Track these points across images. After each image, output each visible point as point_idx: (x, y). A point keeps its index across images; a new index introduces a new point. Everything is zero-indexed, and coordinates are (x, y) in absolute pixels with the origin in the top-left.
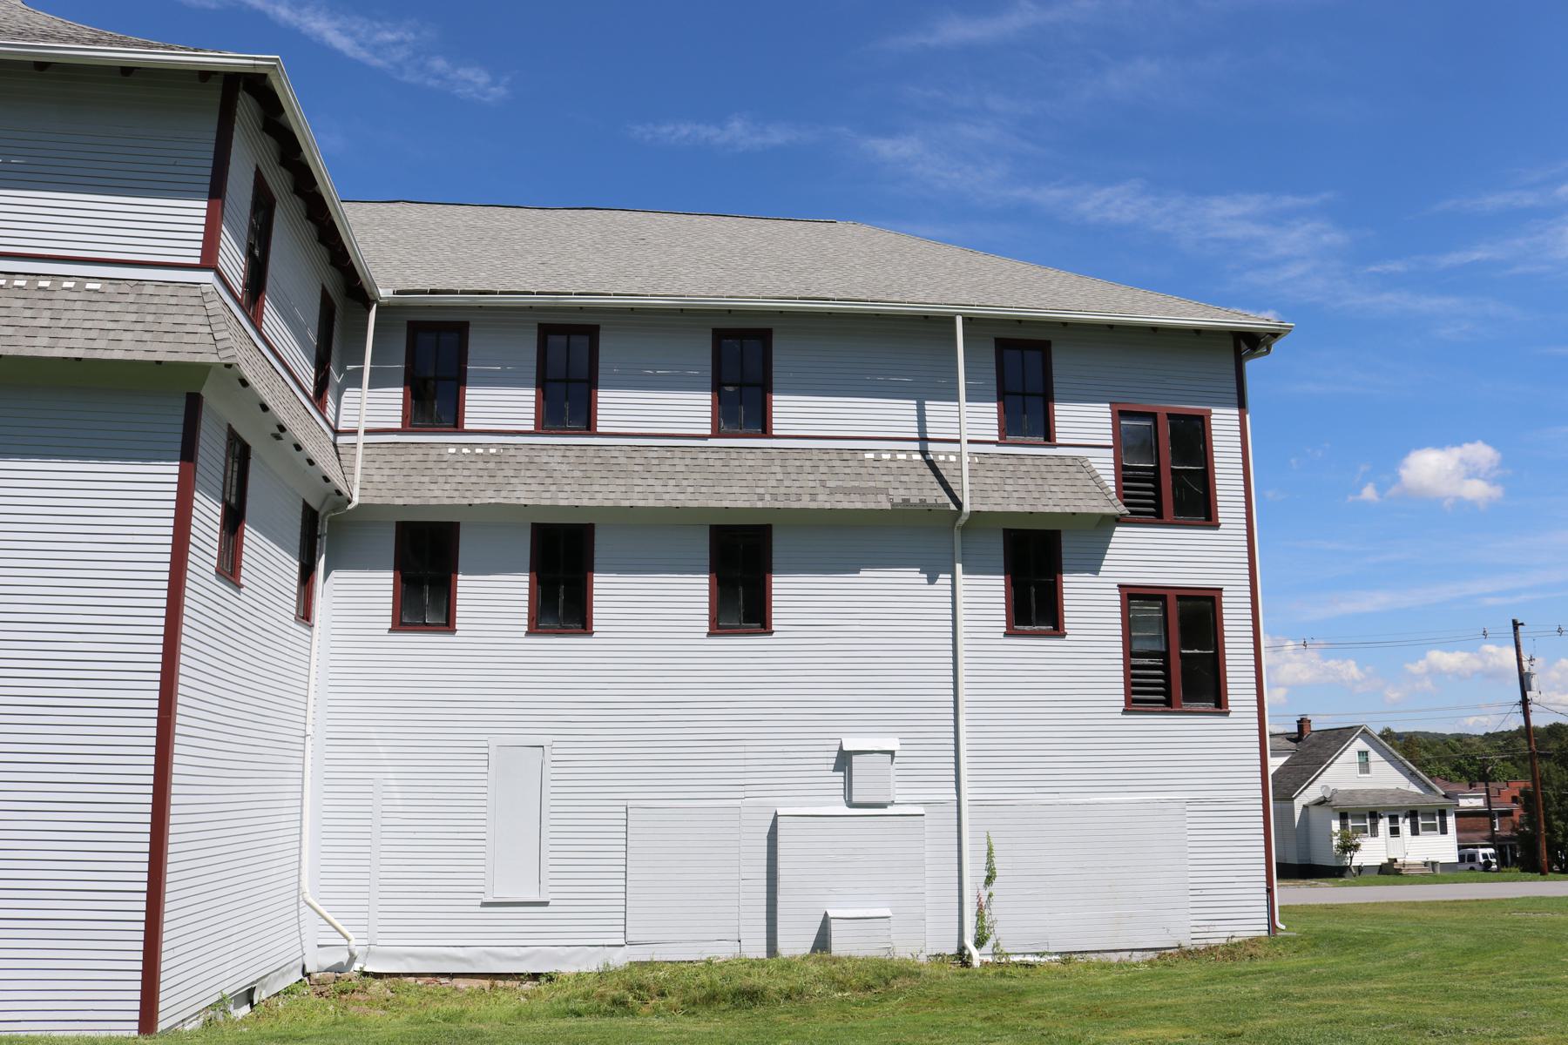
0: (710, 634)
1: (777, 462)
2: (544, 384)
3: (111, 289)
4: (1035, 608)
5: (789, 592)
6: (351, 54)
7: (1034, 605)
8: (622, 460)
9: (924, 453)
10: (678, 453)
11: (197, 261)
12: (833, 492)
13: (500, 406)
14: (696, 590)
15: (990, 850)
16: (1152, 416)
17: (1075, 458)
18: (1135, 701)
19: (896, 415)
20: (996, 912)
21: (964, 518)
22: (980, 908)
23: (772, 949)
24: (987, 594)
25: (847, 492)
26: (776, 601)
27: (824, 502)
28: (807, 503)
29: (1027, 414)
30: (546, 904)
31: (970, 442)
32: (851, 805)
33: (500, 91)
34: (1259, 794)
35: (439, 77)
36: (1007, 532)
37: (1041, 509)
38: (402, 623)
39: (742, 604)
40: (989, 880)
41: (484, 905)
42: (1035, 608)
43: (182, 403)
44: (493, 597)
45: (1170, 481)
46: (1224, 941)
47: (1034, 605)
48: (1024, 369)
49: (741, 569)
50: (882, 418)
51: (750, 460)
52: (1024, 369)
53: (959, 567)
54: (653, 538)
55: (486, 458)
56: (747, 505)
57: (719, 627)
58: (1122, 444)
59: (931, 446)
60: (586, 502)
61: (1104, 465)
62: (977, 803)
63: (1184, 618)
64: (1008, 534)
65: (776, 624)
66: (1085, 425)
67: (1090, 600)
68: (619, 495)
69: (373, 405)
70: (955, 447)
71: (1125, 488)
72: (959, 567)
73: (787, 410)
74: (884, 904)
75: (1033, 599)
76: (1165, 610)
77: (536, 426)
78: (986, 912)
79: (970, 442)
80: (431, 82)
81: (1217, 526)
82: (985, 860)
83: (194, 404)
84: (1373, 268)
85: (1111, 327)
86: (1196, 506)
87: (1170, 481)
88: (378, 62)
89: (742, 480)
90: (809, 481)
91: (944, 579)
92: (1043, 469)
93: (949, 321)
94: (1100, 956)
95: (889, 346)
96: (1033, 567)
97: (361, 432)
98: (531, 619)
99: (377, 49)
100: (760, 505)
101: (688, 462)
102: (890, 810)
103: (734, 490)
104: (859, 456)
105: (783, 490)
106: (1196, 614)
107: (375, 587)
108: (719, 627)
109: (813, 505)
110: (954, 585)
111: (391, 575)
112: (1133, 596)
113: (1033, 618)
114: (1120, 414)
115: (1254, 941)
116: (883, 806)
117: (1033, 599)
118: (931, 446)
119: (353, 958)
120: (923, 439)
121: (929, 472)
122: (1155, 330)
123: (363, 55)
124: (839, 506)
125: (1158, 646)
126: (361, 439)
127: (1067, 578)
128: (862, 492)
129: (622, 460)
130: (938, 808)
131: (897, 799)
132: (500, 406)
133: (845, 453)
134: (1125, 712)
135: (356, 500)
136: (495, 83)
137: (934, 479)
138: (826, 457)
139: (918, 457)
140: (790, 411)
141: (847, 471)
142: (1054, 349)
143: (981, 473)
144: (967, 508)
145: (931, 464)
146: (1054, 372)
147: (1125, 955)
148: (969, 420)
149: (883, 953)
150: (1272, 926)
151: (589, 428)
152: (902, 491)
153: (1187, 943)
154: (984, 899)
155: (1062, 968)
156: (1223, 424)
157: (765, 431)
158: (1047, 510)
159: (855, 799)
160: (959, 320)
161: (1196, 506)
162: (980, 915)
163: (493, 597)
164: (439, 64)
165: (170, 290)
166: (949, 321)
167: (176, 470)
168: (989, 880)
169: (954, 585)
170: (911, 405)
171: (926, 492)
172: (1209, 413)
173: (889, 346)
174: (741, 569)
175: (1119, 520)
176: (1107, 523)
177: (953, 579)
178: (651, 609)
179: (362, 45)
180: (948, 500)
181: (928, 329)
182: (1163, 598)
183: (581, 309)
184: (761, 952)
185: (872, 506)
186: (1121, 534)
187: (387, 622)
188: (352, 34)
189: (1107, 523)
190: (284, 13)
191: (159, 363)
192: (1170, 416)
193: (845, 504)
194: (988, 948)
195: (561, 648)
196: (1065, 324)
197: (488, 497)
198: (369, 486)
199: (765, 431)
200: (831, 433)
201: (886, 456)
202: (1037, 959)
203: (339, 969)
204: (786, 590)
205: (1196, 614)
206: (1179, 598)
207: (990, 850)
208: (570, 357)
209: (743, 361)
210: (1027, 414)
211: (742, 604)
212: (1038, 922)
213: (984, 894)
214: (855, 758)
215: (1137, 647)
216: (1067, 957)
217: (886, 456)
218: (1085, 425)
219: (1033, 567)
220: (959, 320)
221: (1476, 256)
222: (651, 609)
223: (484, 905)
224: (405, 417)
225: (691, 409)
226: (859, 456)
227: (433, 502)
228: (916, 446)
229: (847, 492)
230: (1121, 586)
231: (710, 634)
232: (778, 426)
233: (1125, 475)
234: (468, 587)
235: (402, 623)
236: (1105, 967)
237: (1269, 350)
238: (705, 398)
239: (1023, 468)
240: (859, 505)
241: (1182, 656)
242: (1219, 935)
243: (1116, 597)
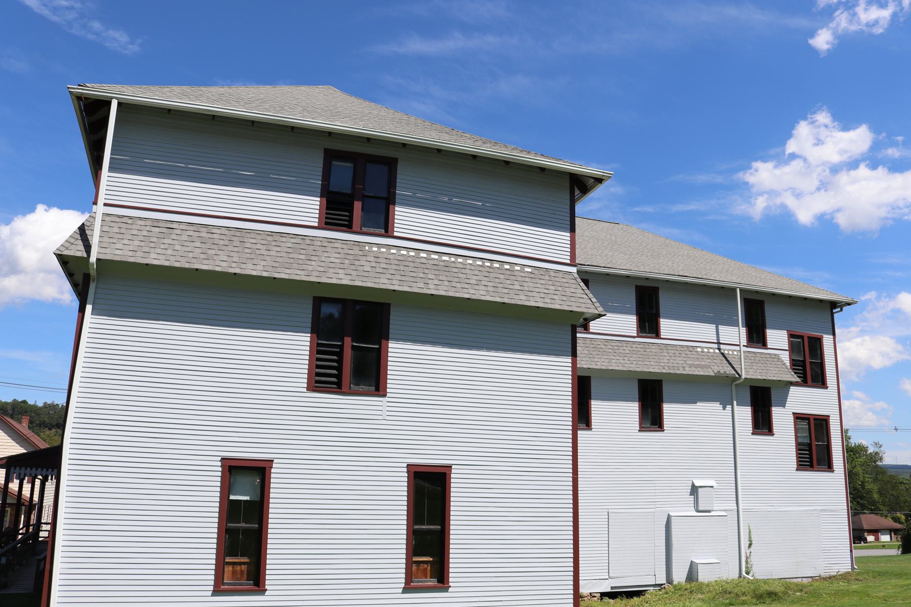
3: (536, 272)
4: (763, 424)
6: (38, 11)
8: (603, 346)
9: (719, 349)
11: (316, 225)
14: (633, 408)
16: (802, 337)
20: (753, 560)
21: (738, 382)
22: (747, 558)
23: (669, 580)
24: (744, 414)
25: (697, 366)
27: (688, 371)
33: (135, 48)
35: (96, 33)
36: (751, 387)
39: (652, 419)
40: (750, 545)
42: (763, 424)
45: (810, 367)
48: (757, 313)
50: (703, 331)
51: (654, 349)
52: (757, 313)
53: (735, 402)
54: (616, 384)
58: (793, 348)
59: (722, 347)
61: (785, 357)
62: (745, 511)
67: (782, 418)
70: (738, 348)
71: (318, 360)
72: (735, 402)
73: (667, 326)
76: (809, 424)
80: (90, 36)
81: (827, 388)
84: (636, 209)
85: (790, 297)
88: (55, 18)
89: (650, 359)
91: (729, 408)
93: (734, 290)
95: (707, 299)
96: (762, 401)
99: (55, 10)
100: (664, 371)
109: (685, 372)
110: (733, 411)
112: (798, 417)
114: (791, 336)
115: (848, 573)
116: (709, 511)
118: (722, 347)
120: (719, 343)
122: (806, 299)
123: (46, 12)
127: (773, 409)
129: (603, 346)
131: (715, 508)
133: (688, 348)
134: (797, 470)
136: (132, 43)
139: (717, 351)
142: (660, 291)
144: (743, 377)
145: (723, 354)
148: (735, 335)
150: (852, 566)
153: (823, 575)
156: (827, 340)
159: (700, 509)
162: (747, 562)
164: (96, 25)
165: (560, 275)
166: (734, 290)
167: (309, 339)
168: (750, 545)
169: (733, 411)
170: (713, 327)
173: (707, 299)
174: (651, 398)
177: (733, 408)
179: (45, 5)
181: (726, 292)
182: (808, 419)
184: (662, 579)
186: (793, 389)
191: (235, 274)
194: (751, 574)
196: (774, 294)
199: (657, 335)
204: (669, 409)
206: (815, 419)
211: (652, 419)
212: (770, 566)
213: (748, 552)
214: (700, 490)
215: (800, 440)
218: (777, 338)
219: (762, 401)
221: (691, 207)
225: (627, 323)
228: (716, 346)
229: (697, 366)
230: (794, 413)
232: (663, 333)
233: (794, 363)
237: (842, 310)
238: (743, 331)
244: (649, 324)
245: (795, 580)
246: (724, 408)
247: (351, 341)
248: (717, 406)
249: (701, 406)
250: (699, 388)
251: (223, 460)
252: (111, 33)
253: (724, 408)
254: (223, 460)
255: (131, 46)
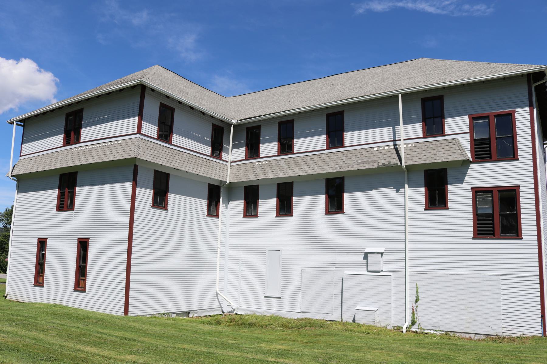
0: (326, 214)
1: (345, 155)
2: (425, 120)
4: (437, 199)
5: (350, 199)
7: (437, 198)
9: (395, 145)
10: (316, 156)
12: (360, 163)
13: (269, 148)
14: (321, 200)
15: (417, 290)
16: (487, 117)
17: (453, 139)
18: (478, 234)
19: (384, 134)
24: (417, 195)
26: (346, 202)
28: (350, 169)
29: (434, 126)
30: (280, 298)
31: (404, 140)
32: (369, 271)
33: (491, 10)
34: (538, 274)
37: (433, 161)
38: (246, 215)
39: (335, 205)
40: (417, 301)
41: (265, 297)
42: (437, 199)
43: (133, 167)
44: (268, 205)
46: (519, 336)
47: (437, 198)
48: (431, 108)
49: (335, 192)
51: (337, 156)
53: (406, 186)
54: (309, 184)
55: (264, 165)
56: (332, 171)
57: (328, 212)
60: (286, 176)
61: (465, 142)
62: (412, 272)
63: (502, 199)
64: (426, 172)
65: (345, 210)
66: (457, 126)
67: (459, 195)
68: (296, 172)
69: (235, 154)
74: (380, 307)
75: (437, 196)
76: (492, 197)
77: (423, 135)
78: (415, 313)
79: (404, 140)
80: (464, 14)
82: (415, 293)
83: (136, 168)
86: (510, 153)
87: (494, 144)
88: (445, 12)
89: (335, 163)
90: (353, 161)
91: (402, 190)
92: (439, 145)
94: (462, 334)
95: (378, 110)
96: (436, 185)
97: (402, 140)
98: (277, 212)
99: (443, 8)
100: (335, 171)
101: (318, 159)
102: (381, 274)
103: (329, 167)
104: (372, 150)
105: (344, 165)
106: (508, 197)
107: (238, 205)
108: (328, 212)
111: (243, 201)
112: (477, 192)
113: (437, 203)
114: (473, 118)
116: (379, 272)
117: (437, 196)
119: (234, 310)
120: (395, 140)
121: (395, 152)
122: (484, 82)
123: (439, 11)
124: (360, 168)
125: (490, 211)
126: (402, 142)
128: (369, 162)
130: (398, 274)
131: (384, 270)
132: (269, 148)
135: (228, 182)
136: (489, 8)
137: (396, 155)
138: (361, 151)
140: (350, 137)
141: (367, 155)
143: (414, 150)
144: (404, 164)
146: (445, 107)
147: (472, 336)
148: (411, 131)
149: (372, 324)
151: (442, 133)
152: (383, 161)
153: (500, 334)
154: (415, 308)
155: (445, 336)
157: (443, 134)
158: (435, 161)
160: (400, 96)
161: (510, 153)
162: (413, 313)
163: (268, 205)
164: (467, 7)
166: (397, 96)
168: (417, 301)
170: (390, 129)
171: (391, 160)
172: (515, 111)
173: (378, 110)
174: (335, 192)
175: (472, 162)
176: (465, 164)
178: (310, 206)
179: (438, 8)
180: (398, 162)
183: (286, 115)
185: (371, 167)
186: (472, 166)
187: (242, 215)
188: (434, 6)
189: (465, 164)
190: (410, 5)
192: (496, 116)
193: (362, 167)
195: (43, 236)
197: (262, 177)
198: (408, 156)
199: (443, 134)
200: (365, 142)
201: (387, 148)
202: (435, 332)
203: (231, 312)
205: (508, 197)
206: (499, 191)
207: (417, 290)
208: (286, 130)
209: (334, 123)
210: (434, 126)
211: (335, 205)
213: (415, 306)
214: (369, 255)
216: (447, 333)
217: (381, 148)
218: (457, 126)
220: (400, 96)
222: (310, 206)
223: (265, 297)
224: (424, 133)
225: (321, 141)
226: (372, 150)
227: (249, 180)
228: (392, 143)
229: (363, 163)
230: (472, 188)
231: (326, 214)
234: (262, 203)
235: (246, 215)
236: (470, 339)
239: (431, 146)
240: (367, 167)
241: (500, 215)
242: (517, 332)
243: (469, 194)
244: (335, 139)
245: (457, 335)
246: (397, 191)
247: (66, 184)
248: (391, 191)
249: (376, 192)
250: (190, 185)
251: (38, 239)
252: (476, 7)
253: (397, 191)
254: (38, 239)
255: (488, 10)
